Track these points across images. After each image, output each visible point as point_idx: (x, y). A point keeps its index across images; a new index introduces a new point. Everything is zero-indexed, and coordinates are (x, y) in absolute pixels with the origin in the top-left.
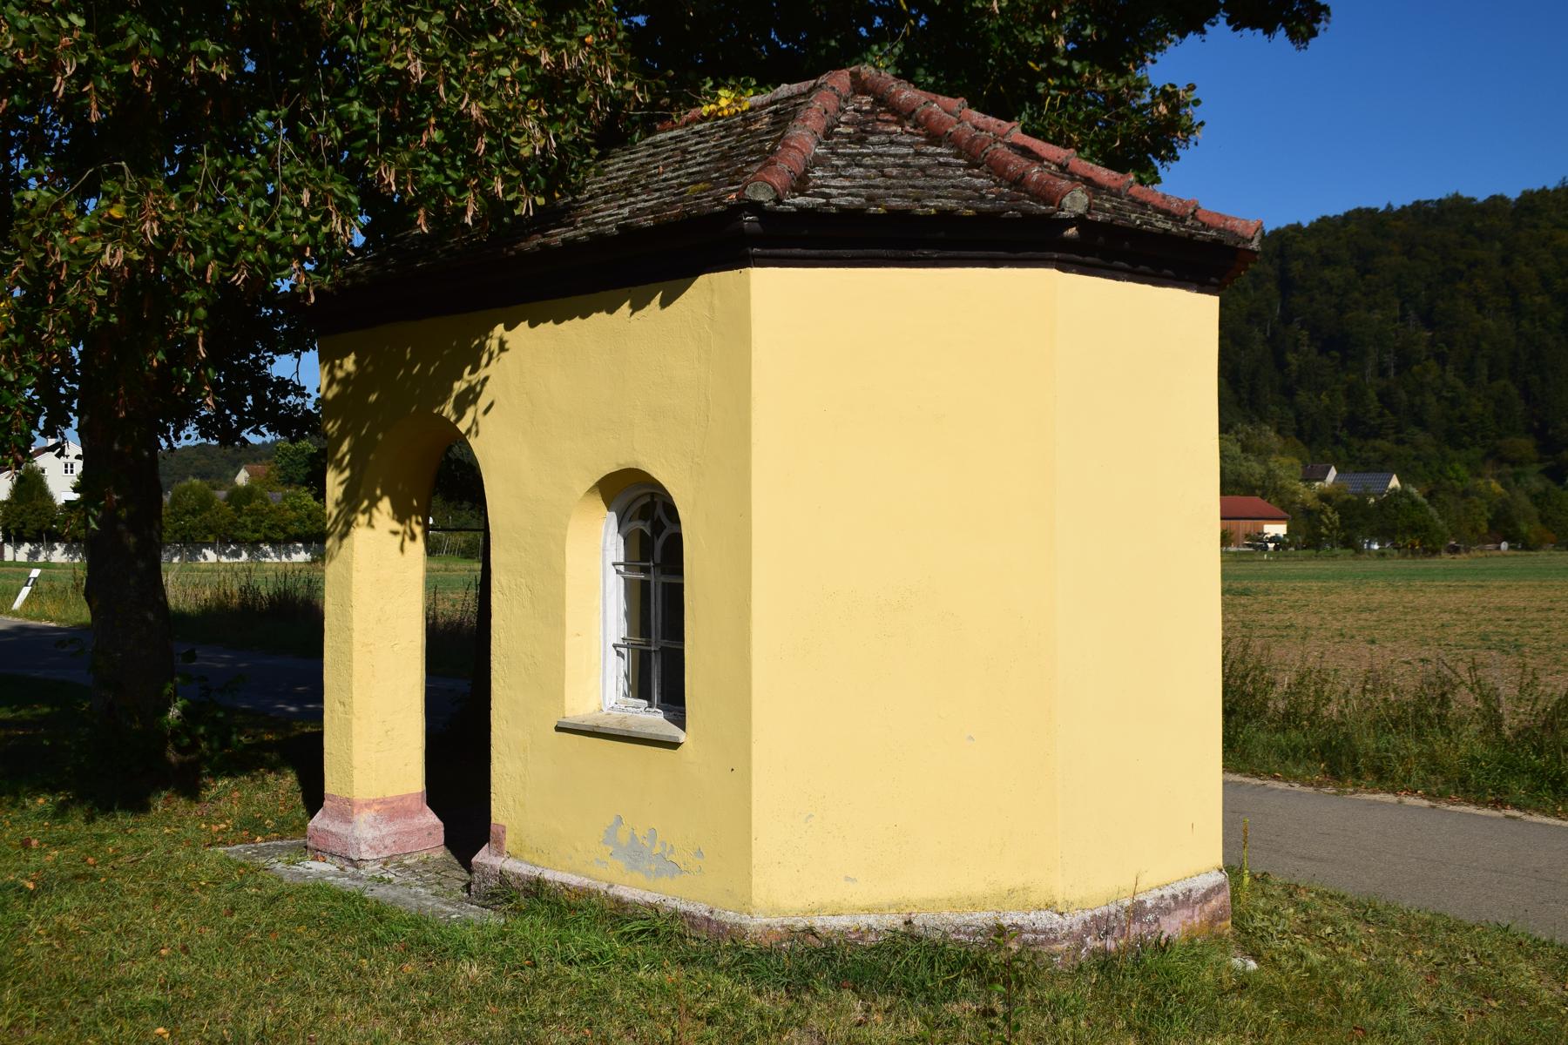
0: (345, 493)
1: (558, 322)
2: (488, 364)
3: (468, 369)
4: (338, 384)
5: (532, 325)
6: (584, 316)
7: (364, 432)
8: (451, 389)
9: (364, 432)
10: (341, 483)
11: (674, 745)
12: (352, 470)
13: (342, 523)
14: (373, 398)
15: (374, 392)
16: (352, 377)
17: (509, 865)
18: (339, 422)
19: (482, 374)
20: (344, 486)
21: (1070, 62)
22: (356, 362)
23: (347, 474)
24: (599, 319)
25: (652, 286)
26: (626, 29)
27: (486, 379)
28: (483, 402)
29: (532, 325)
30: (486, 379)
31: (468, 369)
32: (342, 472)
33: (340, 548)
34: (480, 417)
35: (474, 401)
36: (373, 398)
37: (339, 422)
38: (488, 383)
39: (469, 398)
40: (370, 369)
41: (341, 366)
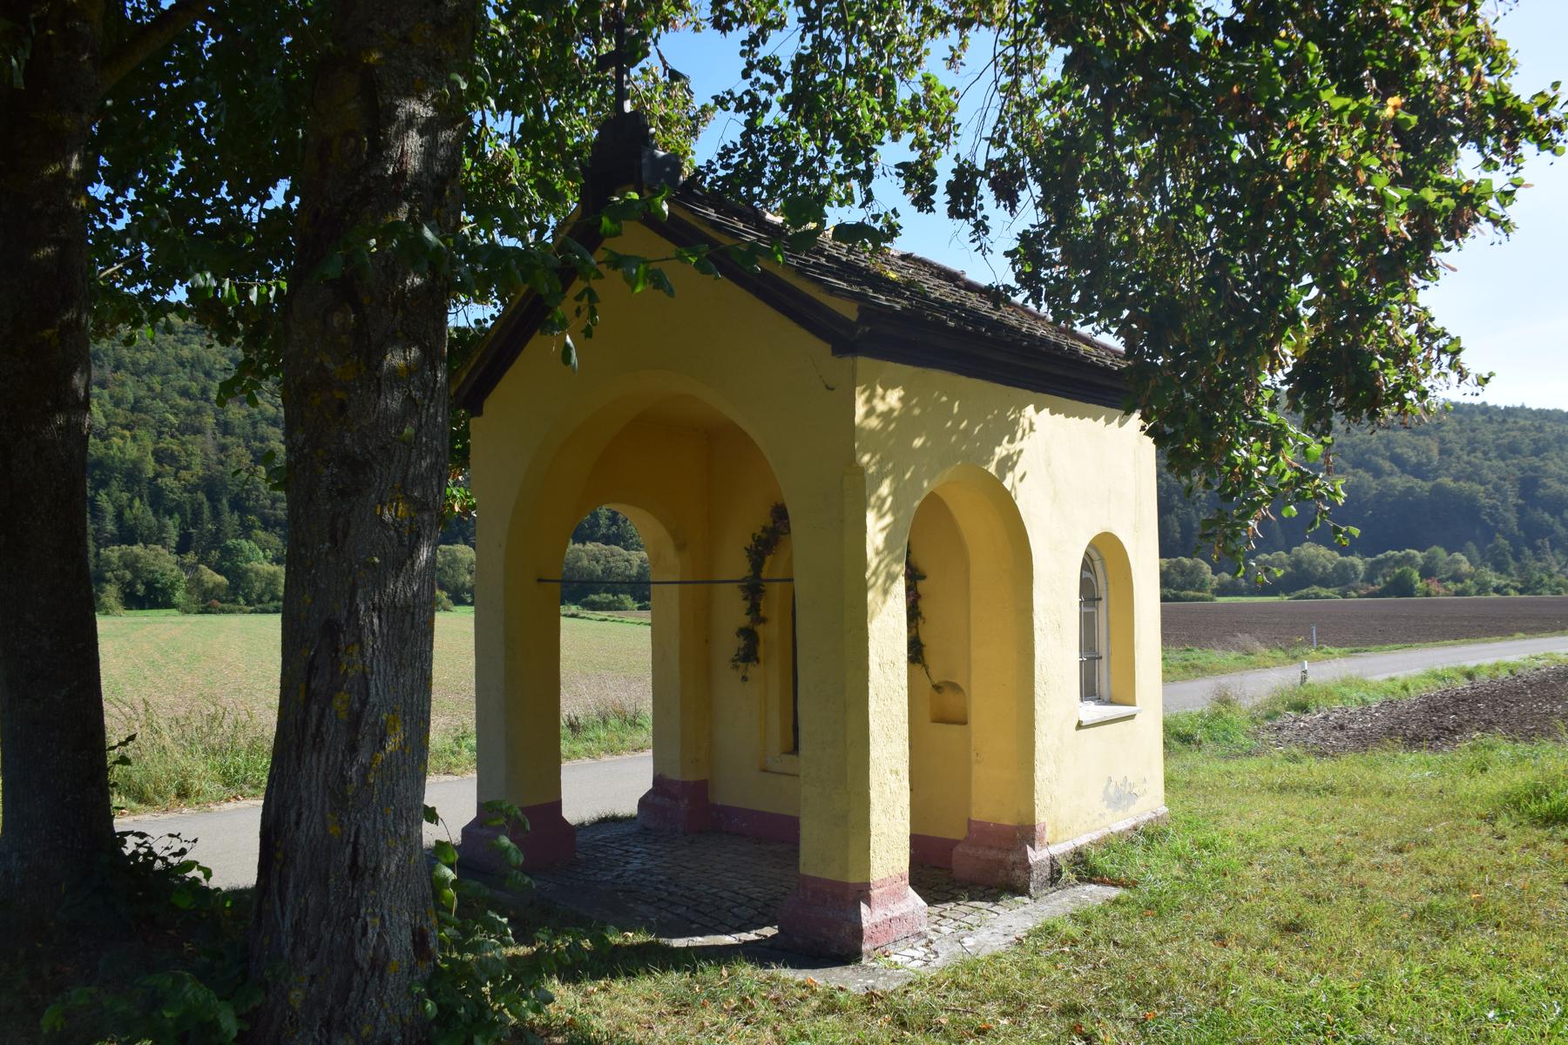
0: (887, 540)
1: (1067, 416)
2: (1022, 439)
3: (1006, 438)
4: (421, 133)
5: (1052, 413)
6: (1082, 418)
7: (908, 475)
8: (993, 453)
9: (908, 475)
10: (883, 529)
11: (1132, 717)
12: (894, 514)
13: (884, 574)
14: (918, 442)
15: (920, 436)
16: (896, 414)
17: (1055, 850)
18: (878, 457)
19: (1017, 446)
20: (885, 533)
21: (234, 320)
22: (901, 399)
23: (888, 519)
24: (1088, 421)
25: (891, 367)
26: (1363, 94)
27: (1021, 451)
28: (1019, 470)
29: (1052, 413)
30: (1021, 451)
31: (1006, 438)
32: (882, 516)
33: (884, 602)
34: (1017, 484)
35: (1012, 468)
36: (918, 442)
37: (878, 457)
38: (1023, 455)
39: (1007, 464)
40: (917, 411)
41: (883, 398)
